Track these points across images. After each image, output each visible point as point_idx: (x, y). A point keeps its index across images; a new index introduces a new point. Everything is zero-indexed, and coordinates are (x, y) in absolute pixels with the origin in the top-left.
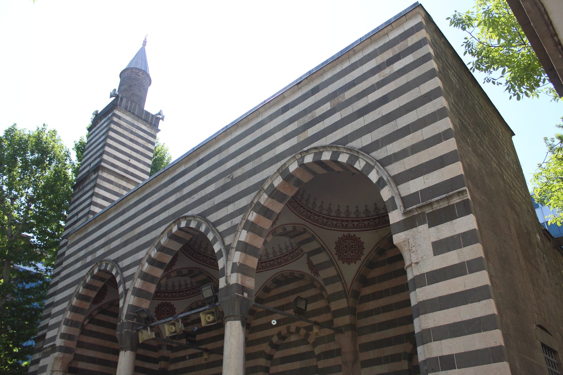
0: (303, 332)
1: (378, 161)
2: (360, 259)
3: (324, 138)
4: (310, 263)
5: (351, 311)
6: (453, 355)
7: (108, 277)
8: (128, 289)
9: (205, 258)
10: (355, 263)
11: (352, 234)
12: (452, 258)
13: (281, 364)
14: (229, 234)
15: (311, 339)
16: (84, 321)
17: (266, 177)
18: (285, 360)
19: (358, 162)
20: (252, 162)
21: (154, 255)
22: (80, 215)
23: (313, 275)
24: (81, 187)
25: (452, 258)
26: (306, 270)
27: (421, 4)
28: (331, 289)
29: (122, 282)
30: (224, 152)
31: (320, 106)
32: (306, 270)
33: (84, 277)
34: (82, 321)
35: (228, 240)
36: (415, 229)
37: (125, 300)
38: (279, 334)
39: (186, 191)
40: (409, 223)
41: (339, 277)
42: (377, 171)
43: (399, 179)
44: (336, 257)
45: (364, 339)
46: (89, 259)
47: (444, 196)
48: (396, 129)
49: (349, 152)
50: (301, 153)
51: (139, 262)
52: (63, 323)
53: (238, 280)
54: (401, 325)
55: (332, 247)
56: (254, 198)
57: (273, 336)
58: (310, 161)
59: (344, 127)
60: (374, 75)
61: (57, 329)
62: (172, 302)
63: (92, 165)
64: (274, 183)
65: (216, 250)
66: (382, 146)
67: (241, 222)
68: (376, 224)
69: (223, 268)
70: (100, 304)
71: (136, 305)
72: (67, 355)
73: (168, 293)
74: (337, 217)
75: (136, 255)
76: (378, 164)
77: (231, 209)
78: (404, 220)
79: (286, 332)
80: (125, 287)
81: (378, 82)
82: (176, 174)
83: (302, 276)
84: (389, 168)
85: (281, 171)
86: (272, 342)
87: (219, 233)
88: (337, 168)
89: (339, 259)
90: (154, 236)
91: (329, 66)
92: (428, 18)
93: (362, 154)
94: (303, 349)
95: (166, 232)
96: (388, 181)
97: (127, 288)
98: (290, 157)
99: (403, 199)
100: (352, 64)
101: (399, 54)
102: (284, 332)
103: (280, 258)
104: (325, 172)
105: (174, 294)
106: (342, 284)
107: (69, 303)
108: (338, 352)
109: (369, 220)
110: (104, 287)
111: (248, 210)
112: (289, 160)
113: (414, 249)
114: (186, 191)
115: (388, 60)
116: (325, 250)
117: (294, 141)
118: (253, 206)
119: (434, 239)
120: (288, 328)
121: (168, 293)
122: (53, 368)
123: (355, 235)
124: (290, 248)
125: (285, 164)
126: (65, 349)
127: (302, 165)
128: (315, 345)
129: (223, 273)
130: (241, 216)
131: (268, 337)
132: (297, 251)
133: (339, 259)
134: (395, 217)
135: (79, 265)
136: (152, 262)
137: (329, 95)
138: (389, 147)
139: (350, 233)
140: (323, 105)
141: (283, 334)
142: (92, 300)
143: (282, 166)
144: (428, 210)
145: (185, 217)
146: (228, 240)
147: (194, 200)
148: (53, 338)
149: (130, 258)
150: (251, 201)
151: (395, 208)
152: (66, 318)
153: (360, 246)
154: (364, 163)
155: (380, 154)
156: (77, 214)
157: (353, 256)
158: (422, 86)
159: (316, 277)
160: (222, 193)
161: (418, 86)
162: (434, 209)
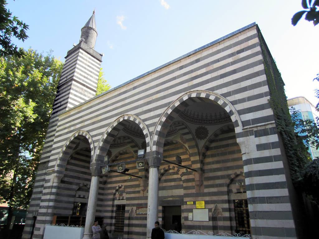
0: (176, 169)
1: (230, 102)
8: (96, 147)
10: (204, 140)
11: (203, 126)
12: (266, 153)
13: (165, 182)
14: (152, 126)
15: (180, 173)
17: (171, 101)
22: (62, 103)
25: (266, 153)
27: (257, 25)
29: (92, 142)
33: (70, 137)
36: (248, 137)
40: (245, 134)
42: (230, 107)
44: (195, 137)
46: (72, 128)
51: (102, 134)
52: (58, 159)
55: (194, 131)
60: (230, 57)
61: (55, 162)
65: (145, 134)
66: (232, 95)
71: (100, 154)
72: (61, 175)
76: (230, 103)
79: (167, 168)
80: (94, 145)
81: (232, 62)
85: (179, 99)
87: (146, 125)
92: (259, 35)
93: (222, 97)
94: (175, 176)
95: (117, 121)
96: (235, 112)
99: (243, 122)
112: (184, 95)
113: (247, 146)
115: (237, 51)
119: (258, 143)
120: (169, 166)
122: (53, 181)
130: (158, 118)
134: (238, 130)
135: (66, 131)
138: (236, 95)
139: (202, 126)
144: (255, 129)
145: (127, 115)
148: (53, 166)
151: (238, 125)
152: (60, 157)
156: (60, 102)
160: (147, 105)
162: (258, 129)
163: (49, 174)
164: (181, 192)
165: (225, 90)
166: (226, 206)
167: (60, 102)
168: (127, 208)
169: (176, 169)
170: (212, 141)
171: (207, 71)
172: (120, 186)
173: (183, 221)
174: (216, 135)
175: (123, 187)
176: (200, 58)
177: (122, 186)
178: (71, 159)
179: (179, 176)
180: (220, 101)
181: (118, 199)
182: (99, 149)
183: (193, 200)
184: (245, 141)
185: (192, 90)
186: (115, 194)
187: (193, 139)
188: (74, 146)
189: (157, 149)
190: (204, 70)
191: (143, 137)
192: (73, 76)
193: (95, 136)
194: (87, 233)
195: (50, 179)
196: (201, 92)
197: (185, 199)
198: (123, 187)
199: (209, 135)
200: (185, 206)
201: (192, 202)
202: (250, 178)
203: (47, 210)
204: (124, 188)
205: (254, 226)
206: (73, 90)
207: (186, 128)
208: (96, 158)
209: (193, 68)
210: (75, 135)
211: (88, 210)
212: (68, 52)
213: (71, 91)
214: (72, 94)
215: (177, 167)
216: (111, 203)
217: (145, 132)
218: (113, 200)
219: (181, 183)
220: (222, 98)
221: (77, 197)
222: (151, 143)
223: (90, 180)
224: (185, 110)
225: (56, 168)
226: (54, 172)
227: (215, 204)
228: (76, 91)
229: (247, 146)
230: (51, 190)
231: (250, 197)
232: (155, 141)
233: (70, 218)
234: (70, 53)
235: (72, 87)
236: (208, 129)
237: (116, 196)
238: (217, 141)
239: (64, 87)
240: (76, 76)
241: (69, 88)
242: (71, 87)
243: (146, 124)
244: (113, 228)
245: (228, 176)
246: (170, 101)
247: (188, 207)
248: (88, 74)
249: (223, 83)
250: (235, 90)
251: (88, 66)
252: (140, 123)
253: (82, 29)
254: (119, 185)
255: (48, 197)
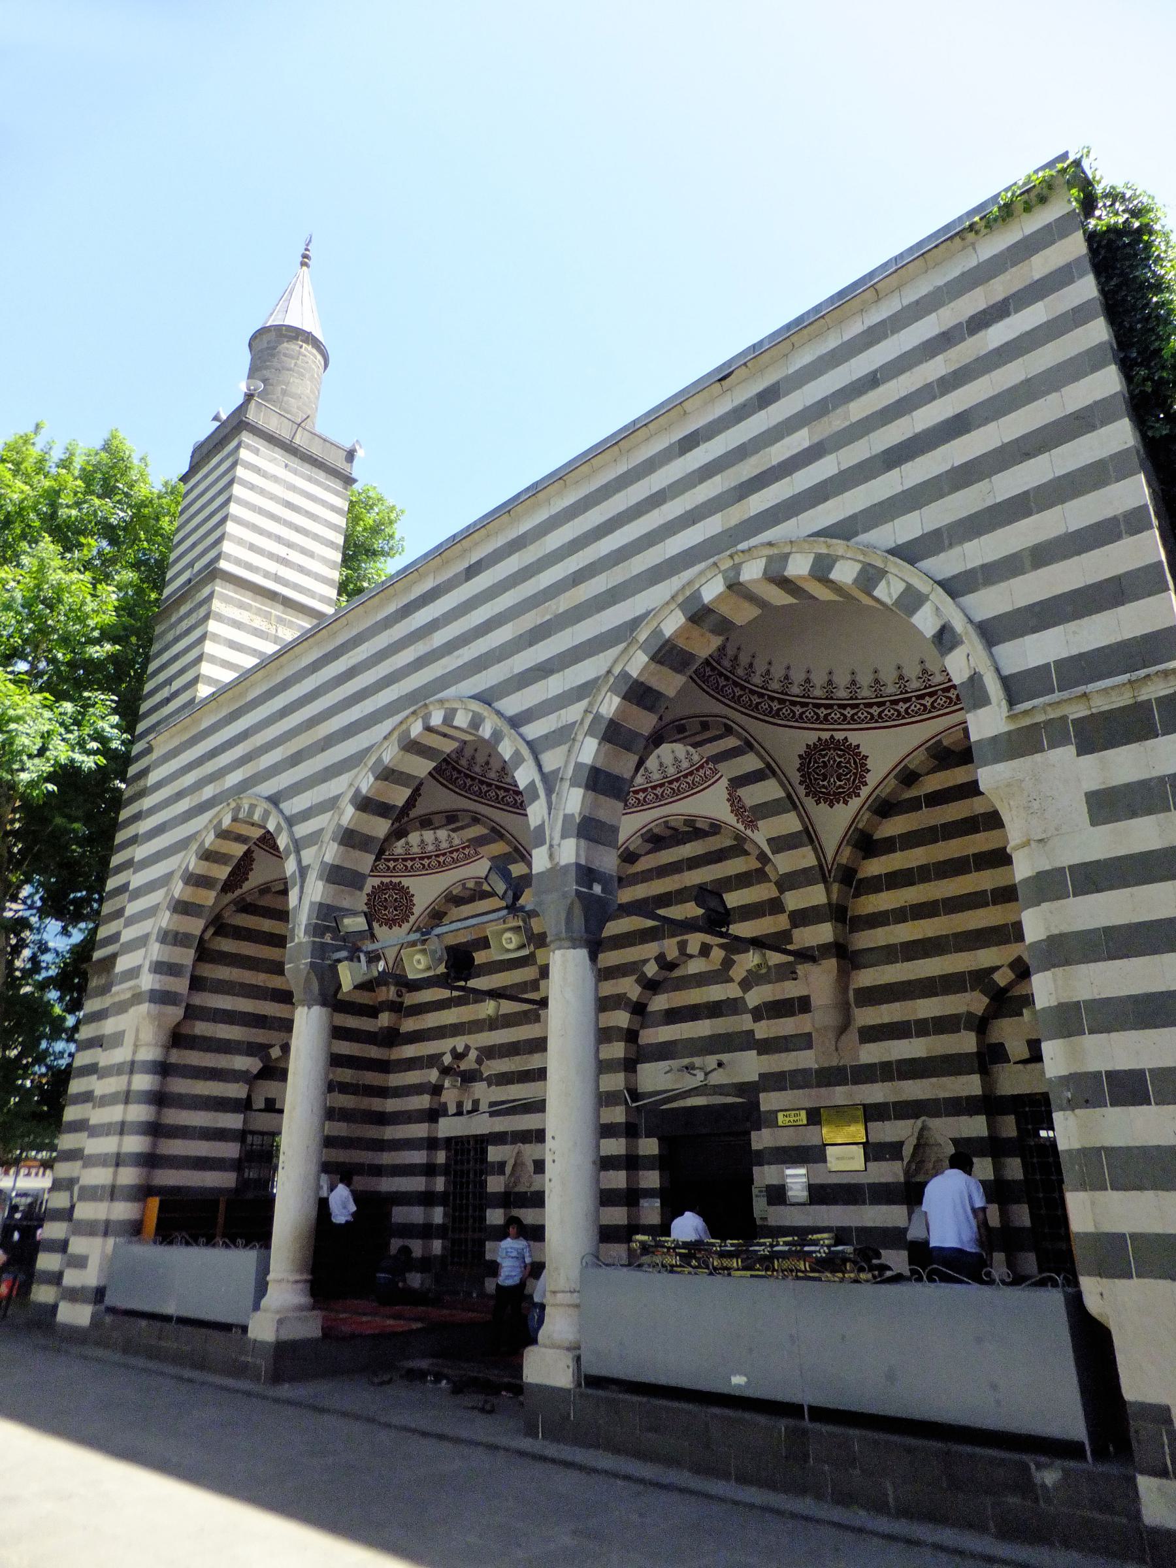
2: (858, 795)
3: (794, 520)
4: (737, 806)
5: (838, 913)
6: (1142, 1072)
7: (257, 833)
9: (484, 788)
11: (839, 736)
16: (204, 931)
17: (644, 611)
18: (673, 1016)
19: (883, 582)
20: (604, 574)
21: (369, 789)
22: (176, 685)
23: (741, 827)
24: (173, 619)
26: (723, 812)
28: (785, 863)
30: (531, 548)
31: (782, 438)
32: (723, 812)
34: (198, 933)
35: (552, 759)
36: (1038, 757)
37: (302, 888)
38: (660, 959)
39: (440, 638)
40: (1022, 742)
41: (809, 836)
43: (992, 633)
44: (801, 790)
45: (867, 978)
46: (208, 792)
47: (1125, 677)
48: (989, 502)
49: (861, 558)
50: (731, 556)
51: (331, 804)
52: (154, 937)
53: (578, 855)
54: (959, 949)
56: (615, 662)
57: (645, 961)
58: (755, 577)
59: (847, 494)
60: (934, 357)
61: (142, 951)
62: (406, 882)
63: (197, 566)
64: (662, 626)
65: (522, 785)
66: (951, 546)
67: (582, 720)
68: (899, 714)
69: (541, 828)
70: (238, 892)
71: (329, 902)
72: (170, 1010)
73: (412, 859)
74: (803, 697)
75: (324, 786)
77: (554, 685)
78: (1009, 733)
80: (299, 861)
82: (413, 597)
83: (715, 828)
84: (969, 600)
85: (680, 599)
86: (643, 974)
88: (822, 593)
89: (807, 795)
90: (366, 745)
91: (805, 332)
94: (716, 993)
95: (396, 735)
97: (304, 863)
98: (703, 565)
99: (1007, 682)
100: (870, 328)
101: (1005, 301)
102: (672, 954)
103: (661, 785)
104: (789, 600)
105: (426, 862)
106: (815, 850)
107: (167, 894)
108: (803, 1005)
109: (883, 703)
110: (248, 855)
111: (599, 690)
112: (701, 573)
113: (1036, 805)
114: (440, 638)
116: (774, 773)
117: (712, 526)
118: (612, 680)
119: (1094, 786)
120: (682, 946)
121: (412, 859)
123: (846, 739)
124: (685, 764)
125: (690, 583)
126: (162, 997)
127: (734, 587)
128: (746, 985)
129: (539, 837)
130: (584, 704)
131: (634, 963)
132: (701, 772)
133: (807, 795)
135: (184, 805)
136: (366, 805)
137: (806, 409)
140: (789, 434)
141: (669, 958)
142: (219, 887)
143: (683, 588)
145: (441, 701)
146: (552, 759)
147: (460, 662)
148: (133, 973)
149: (308, 794)
150: (605, 669)
151: (982, 700)
152: (160, 928)
153: (857, 763)
154: (901, 586)
155: (948, 563)
156: (168, 682)
157: (840, 787)
158: (1068, 390)
159: (749, 832)
160: (531, 645)
161: (1057, 389)
162: (1094, 711)
163: (121, 1008)
164: (748, 1066)
165: (908, 527)
166: (975, 1126)
167: (168, 682)
168: (494, 1153)
169: (718, 954)
170: (885, 808)
171: (816, 440)
172: (460, 1049)
173: (759, 1205)
174: (908, 777)
175: (473, 1054)
176: (778, 383)
177: (467, 1048)
178: (215, 934)
179: (731, 991)
180: (888, 583)
181: (452, 1109)
182: (320, 877)
183: (808, 1105)
184: (1022, 781)
185: (743, 546)
186: (437, 1090)
187: (791, 803)
188: (222, 872)
189: (582, 853)
190: (800, 440)
191: (516, 801)
192: (218, 557)
193: (306, 815)
194: (280, 1276)
195: (124, 1031)
196: (787, 550)
197: (769, 1101)
198: (473, 1054)
199: (872, 779)
200: (765, 1132)
201: (803, 1114)
202: (1059, 971)
203: (115, 1174)
204: (479, 1061)
205: (1090, 1228)
206: (220, 618)
207: (748, 746)
208: (309, 918)
209: (745, 438)
210: (220, 822)
211: (280, 1165)
212: (194, 452)
213: (213, 626)
214: (216, 638)
215: (721, 946)
216: (420, 1130)
217: (524, 776)
218: (433, 1115)
219: (745, 1022)
220: (896, 566)
221: (260, 1110)
222: (552, 829)
223: (287, 1025)
224: (722, 649)
225: (147, 981)
226: (137, 998)
227: (917, 1117)
228: (237, 625)
229: (1036, 805)
230: (129, 1083)
231: (1064, 1072)
232: (573, 815)
233: (222, 1207)
234: (203, 454)
235: (213, 608)
236: (864, 750)
237: (443, 1100)
238: (914, 805)
239: (184, 609)
240: (229, 558)
241: (202, 612)
242: (210, 607)
243: (530, 738)
244: (437, 1246)
245: (981, 978)
246: (637, 614)
247: (784, 1138)
248: (290, 545)
249: (899, 489)
250: (961, 522)
251: (289, 505)
252: (497, 736)
253: (254, 338)
254: (454, 1048)
255: (115, 1113)
